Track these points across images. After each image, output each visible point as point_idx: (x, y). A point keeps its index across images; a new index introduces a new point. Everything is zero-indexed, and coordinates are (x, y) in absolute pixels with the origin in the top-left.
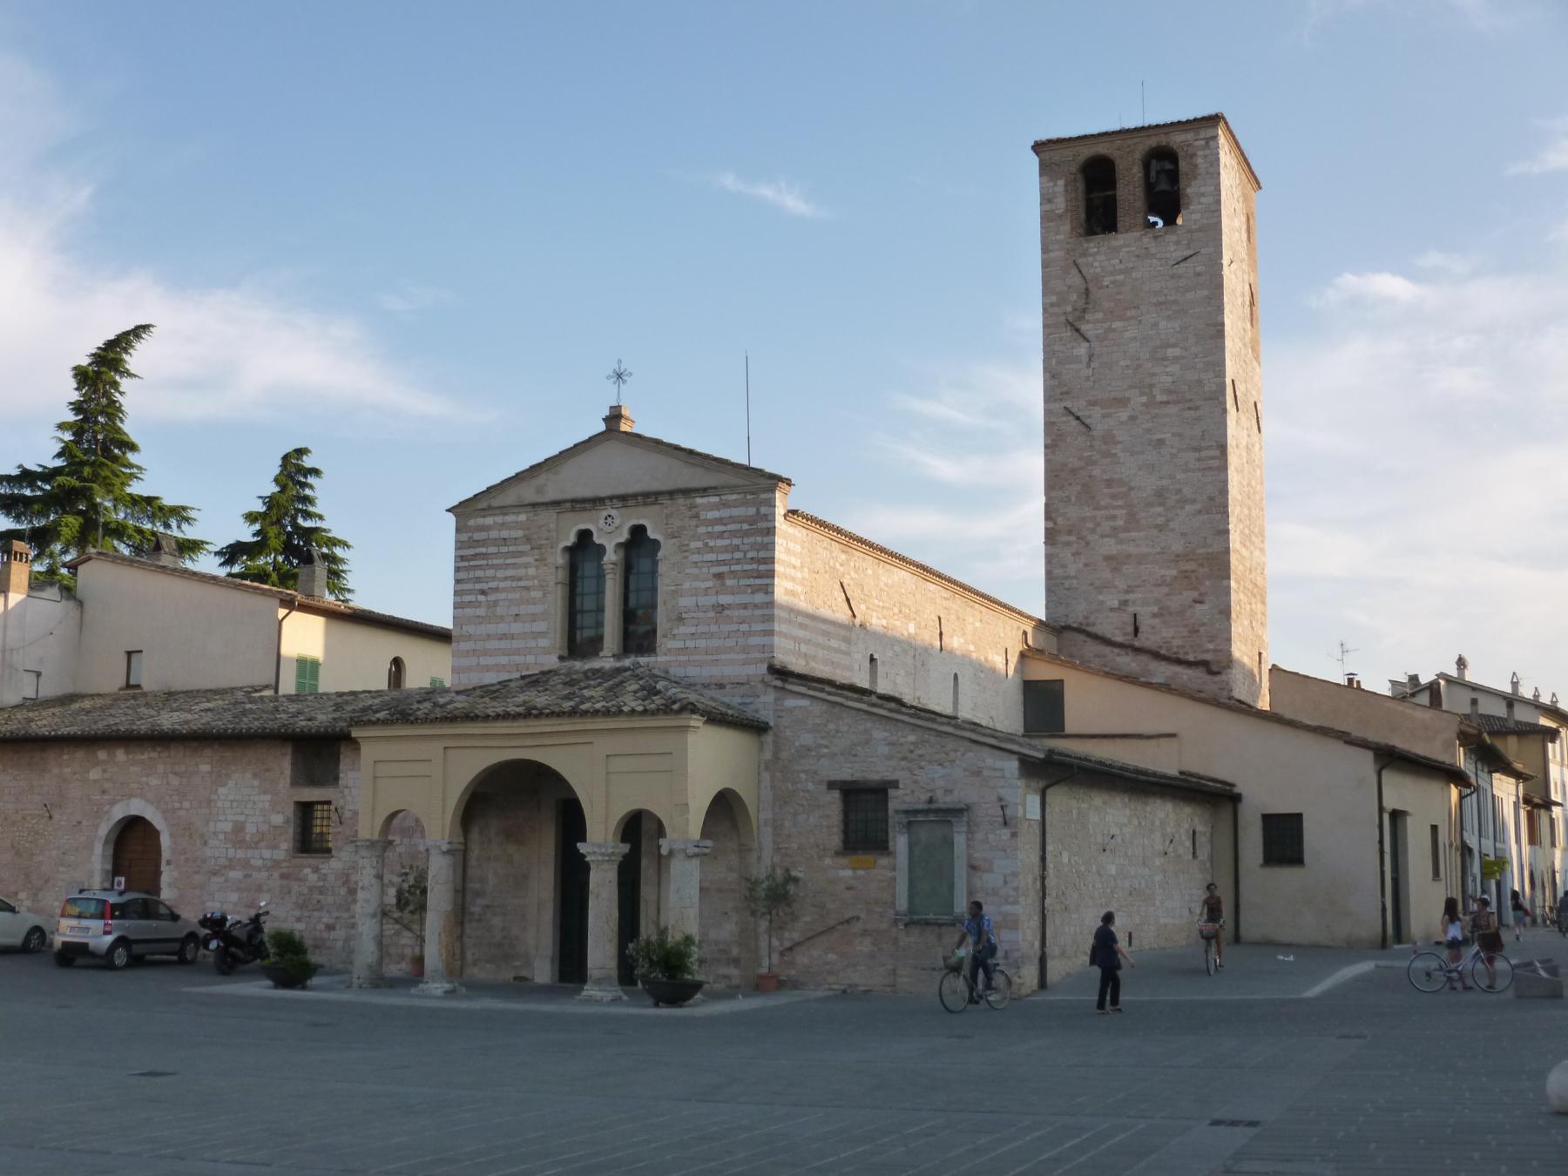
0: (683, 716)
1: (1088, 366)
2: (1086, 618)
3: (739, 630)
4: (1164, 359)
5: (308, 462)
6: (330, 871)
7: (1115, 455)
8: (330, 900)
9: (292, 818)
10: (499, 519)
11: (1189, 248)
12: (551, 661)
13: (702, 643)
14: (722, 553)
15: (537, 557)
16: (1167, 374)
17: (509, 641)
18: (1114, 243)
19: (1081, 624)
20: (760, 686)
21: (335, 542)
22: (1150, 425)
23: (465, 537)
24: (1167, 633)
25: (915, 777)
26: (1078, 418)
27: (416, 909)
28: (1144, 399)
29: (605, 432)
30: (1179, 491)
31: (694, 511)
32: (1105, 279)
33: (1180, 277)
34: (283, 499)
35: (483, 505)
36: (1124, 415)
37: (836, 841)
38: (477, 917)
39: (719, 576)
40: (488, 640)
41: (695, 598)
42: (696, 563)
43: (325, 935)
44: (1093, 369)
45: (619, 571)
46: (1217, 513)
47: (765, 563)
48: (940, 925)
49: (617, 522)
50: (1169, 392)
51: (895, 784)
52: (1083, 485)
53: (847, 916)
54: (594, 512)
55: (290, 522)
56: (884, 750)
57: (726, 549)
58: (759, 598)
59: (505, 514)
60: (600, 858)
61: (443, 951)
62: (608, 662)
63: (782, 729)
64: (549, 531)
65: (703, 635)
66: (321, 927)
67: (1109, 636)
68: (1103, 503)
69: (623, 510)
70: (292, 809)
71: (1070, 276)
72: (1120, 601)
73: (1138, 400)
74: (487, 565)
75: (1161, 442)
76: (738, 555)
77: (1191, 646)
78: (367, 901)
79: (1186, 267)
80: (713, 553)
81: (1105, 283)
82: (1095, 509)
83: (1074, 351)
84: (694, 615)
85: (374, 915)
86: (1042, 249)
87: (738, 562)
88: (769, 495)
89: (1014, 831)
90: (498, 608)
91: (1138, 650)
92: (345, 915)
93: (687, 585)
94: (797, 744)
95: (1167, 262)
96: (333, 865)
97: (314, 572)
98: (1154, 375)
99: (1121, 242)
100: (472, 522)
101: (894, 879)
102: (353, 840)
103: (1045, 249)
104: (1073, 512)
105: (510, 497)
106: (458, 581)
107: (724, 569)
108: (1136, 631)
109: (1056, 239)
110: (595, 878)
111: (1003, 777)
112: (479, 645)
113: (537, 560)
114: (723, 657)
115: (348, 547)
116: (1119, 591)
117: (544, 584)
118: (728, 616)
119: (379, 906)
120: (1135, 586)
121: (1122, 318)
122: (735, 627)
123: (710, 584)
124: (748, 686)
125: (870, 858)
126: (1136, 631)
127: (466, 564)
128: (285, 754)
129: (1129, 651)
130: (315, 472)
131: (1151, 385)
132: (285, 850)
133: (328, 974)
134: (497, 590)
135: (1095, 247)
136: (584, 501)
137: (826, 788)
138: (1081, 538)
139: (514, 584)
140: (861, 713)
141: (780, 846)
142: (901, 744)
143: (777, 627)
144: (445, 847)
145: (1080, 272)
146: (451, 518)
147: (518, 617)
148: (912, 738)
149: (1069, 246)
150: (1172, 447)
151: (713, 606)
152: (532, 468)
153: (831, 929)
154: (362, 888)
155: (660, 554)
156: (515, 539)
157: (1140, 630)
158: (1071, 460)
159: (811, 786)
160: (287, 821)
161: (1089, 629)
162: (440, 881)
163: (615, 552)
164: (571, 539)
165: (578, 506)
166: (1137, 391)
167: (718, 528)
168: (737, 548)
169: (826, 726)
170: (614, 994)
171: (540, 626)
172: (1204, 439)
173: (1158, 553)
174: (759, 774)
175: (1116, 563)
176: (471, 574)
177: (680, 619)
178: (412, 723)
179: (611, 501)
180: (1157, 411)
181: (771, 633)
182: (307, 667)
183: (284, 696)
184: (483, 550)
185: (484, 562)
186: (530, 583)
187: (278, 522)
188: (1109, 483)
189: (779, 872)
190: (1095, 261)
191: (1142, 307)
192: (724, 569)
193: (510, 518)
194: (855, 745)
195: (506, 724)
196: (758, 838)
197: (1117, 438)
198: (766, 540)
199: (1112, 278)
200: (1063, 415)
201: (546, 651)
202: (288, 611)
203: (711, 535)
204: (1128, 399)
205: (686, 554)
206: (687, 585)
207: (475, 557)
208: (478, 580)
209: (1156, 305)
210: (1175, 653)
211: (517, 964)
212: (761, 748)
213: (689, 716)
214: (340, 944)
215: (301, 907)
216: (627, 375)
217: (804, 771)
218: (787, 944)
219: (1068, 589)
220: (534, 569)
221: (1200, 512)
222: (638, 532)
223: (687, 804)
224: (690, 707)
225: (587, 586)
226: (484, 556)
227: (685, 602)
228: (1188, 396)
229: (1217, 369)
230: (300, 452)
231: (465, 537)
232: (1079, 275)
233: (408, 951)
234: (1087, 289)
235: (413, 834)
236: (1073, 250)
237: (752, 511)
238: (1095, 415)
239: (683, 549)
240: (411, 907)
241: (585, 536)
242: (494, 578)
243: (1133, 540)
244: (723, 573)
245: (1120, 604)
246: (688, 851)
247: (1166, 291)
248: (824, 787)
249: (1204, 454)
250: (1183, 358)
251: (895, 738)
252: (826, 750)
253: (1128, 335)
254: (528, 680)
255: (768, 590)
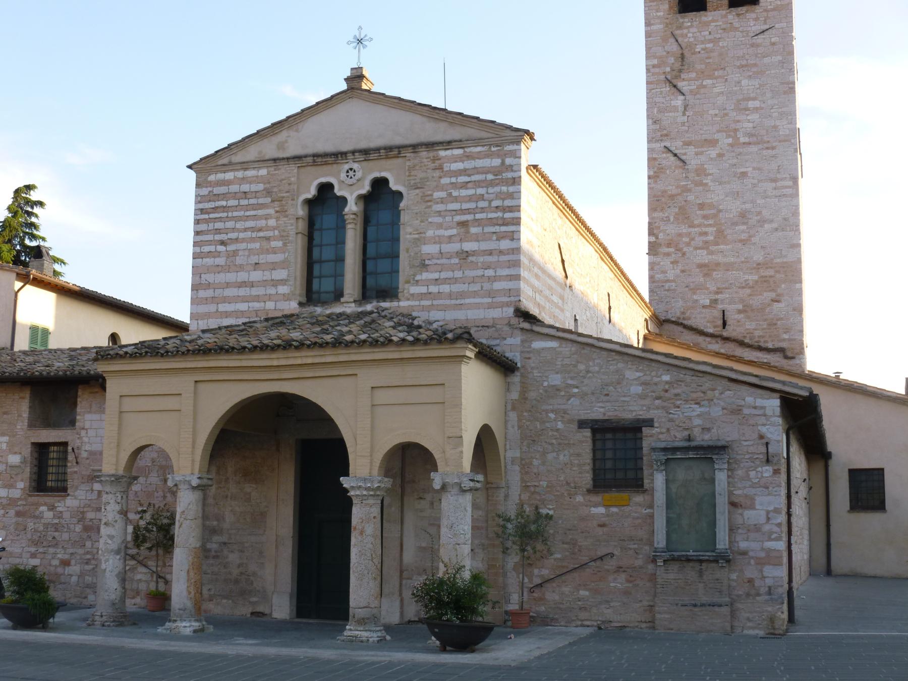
0: (458, 346)
1: (684, 114)
2: (683, 313)
3: (484, 275)
4: (747, 109)
5: (34, 196)
6: (66, 509)
7: (706, 184)
8: (65, 536)
9: (29, 459)
10: (240, 174)
11: (765, 23)
12: (292, 306)
13: (445, 288)
14: (466, 202)
15: (277, 209)
16: (749, 121)
17: (248, 289)
18: (704, 19)
19: (679, 318)
20: (506, 328)
21: (56, 260)
22: (735, 161)
23: (205, 191)
24: (750, 325)
25: (671, 416)
26: (675, 155)
27: (153, 546)
28: (730, 140)
29: (348, 90)
30: (759, 213)
31: (437, 163)
32: (697, 47)
33: (758, 46)
34: (14, 223)
35: (225, 161)
36: (713, 153)
37: (587, 479)
38: (213, 553)
39: (463, 224)
40: (227, 287)
41: (439, 245)
42: (440, 212)
43: (60, 570)
44: (688, 116)
45: (360, 221)
46: (790, 231)
47: (511, 212)
48: (701, 561)
49: (359, 174)
50: (751, 135)
51: (650, 423)
52: (680, 208)
53: (600, 553)
54: (335, 166)
55: (19, 242)
56: (637, 389)
57: (470, 199)
58: (505, 244)
59: (246, 169)
60: (365, 493)
61: (192, 590)
62: (349, 307)
63: (529, 370)
64: (289, 184)
65: (446, 281)
66: (56, 562)
67: (702, 328)
68: (696, 222)
69: (365, 163)
70: (29, 450)
71: (669, 44)
72: (711, 300)
73: (725, 141)
74: (227, 217)
75: (744, 175)
76: (482, 204)
77: (770, 336)
78: (111, 537)
79: (764, 38)
80: (457, 202)
81: (697, 50)
82: (690, 227)
83: (672, 102)
84: (438, 262)
85: (118, 552)
86: (645, 23)
87: (483, 210)
88: (515, 147)
89: (776, 468)
90: (237, 258)
91: (726, 339)
92: (81, 551)
93: (430, 233)
94: (546, 384)
95: (748, 34)
96: (70, 503)
97: (43, 265)
98: (738, 121)
99: (710, 18)
100: (212, 178)
101: (652, 516)
102: (94, 477)
103: (648, 24)
104: (672, 229)
105: (251, 153)
106: (197, 233)
107: (469, 217)
108: (724, 324)
109: (656, 16)
110: (357, 513)
111: (765, 415)
112: (218, 292)
113: (277, 212)
114: (468, 301)
115: (64, 263)
116: (710, 292)
117: (285, 234)
118: (472, 262)
119: (123, 542)
120: (723, 288)
121: (710, 77)
122: (480, 272)
123: (454, 232)
124: (494, 328)
125: (625, 495)
126: (724, 324)
127: (206, 216)
128: (23, 398)
129: (719, 340)
130: (41, 204)
131: (735, 129)
132: (22, 489)
133: (70, 609)
134: (237, 240)
135: (689, 22)
136: (326, 155)
137: (576, 427)
138: (679, 250)
139: (254, 235)
140: (614, 354)
141: (529, 484)
142: (656, 384)
143: (524, 273)
144: (195, 482)
145: (677, 41)
146: (192, 175)
147: (257, 265)
148: (666, 378)
149: (667, 21)
150: (753, 178)
151: (457, 252)
152: (273, 125)
153: (583, 566)
154: (105, 524)
155: (402, 205)
156: (256, 192)
157: (728, 323)
158: (670, 188)
159: (560, 425)
160: (24, 461)
161: (685, 322)
162: (189, 517)
163: (356, 204)
164: (311, 192)
165: (320, 160)
166: (725, 134)
167: (463, 179)
168: (482, 197)
169: (575, 366)
170: (379, 634)
171: (281, 274)
172: (779, 172)
173: (742, 262)
174: (505, 413)
175: (707, 269)
176: (211, 226)
177: (424, 266)
178: (162, 355)
179: (354, 155)
180: (741, 150)
181: (517, 277)
182: (38, 334)
183: (20, 352)
184: (224, 203)
185: (225, 215)
186: (269, 234)
187: (10, 241)
188: (702, 206)
189: (527, 509)
190: (689, 32)
191: (727, 69)
192: (469, 217)
193: (250, 173)
194: (607, 385)
195: (264, 356)
196: (505, 477)
197: (708, 171)
198: (511, 189)
199: (703, 46)
200: (663, 153)
201: (287, 298)
202: (22, 284)
203: (454, 185)
204: (717, 141)
205: (429, 204)
206: (430, 233)
207: (215, 209)
208: (218, 231)
209: (739, 67)
210: (756, 342)
211: (254, 599)
212: (508, 390)
213: (465, 346)
214: (74, 579)
215: (36, 543)
216: (367, 40)
217: (552, 411)
218: (538, 581)
219: (668, 290)
220: (274, 220)
221: (776, 229)
222: (380, 184)
223: (461, 437)
224: (466, 336)
225: (325, 237)
226: (225, 209)
227: (429, 249)
228: (765, 139)
229: (789, 117)
230: (29, 188)
231: (205, 191)
232: (676, 43)
233: (143, 587)
234: (682, 54)
235: (149, 473)
236: (671, 24)
237: (497, 162)
238: (689, 153)
239: (427, 200)
240: (148, 545)
241: (325, 189)
242: (234, 230)
243: (721, 252)
244: (467, 221)
245: (710, 303)
246: (462, 485)
247: (747, 57)
248: (574, 426)
249: (779, 184)
250: (762, 108)
251: (648, 378)
252: (576, 390)
253: (716, 90)
254: (271, 322)
255: (514, 236)
